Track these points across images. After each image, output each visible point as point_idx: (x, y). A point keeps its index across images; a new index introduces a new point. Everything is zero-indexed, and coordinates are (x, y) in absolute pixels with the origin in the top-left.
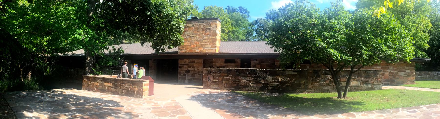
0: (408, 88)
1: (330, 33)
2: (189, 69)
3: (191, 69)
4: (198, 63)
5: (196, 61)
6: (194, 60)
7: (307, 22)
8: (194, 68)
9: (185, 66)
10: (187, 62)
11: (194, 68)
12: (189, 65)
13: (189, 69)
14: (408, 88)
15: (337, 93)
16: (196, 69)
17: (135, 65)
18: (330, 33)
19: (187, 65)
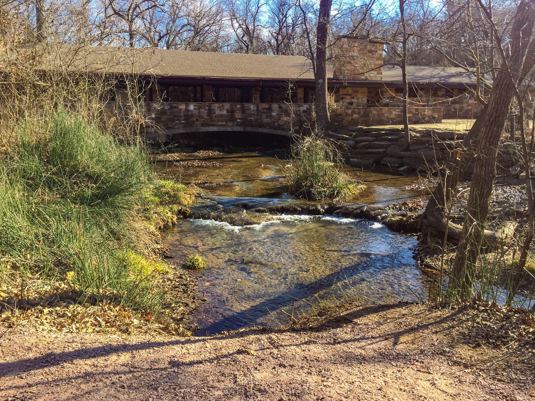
0: (230, 158)
1: (463, 43)
2: (353, 100)
3: (355, 100)
4: (362, 92)
5: (360, 90)
6: (358, 89)
7: (29, 108)
8: (358, 99)
9: (348, 97)
10: (350, 92)
11: (358, 99)
12: (353, 96)
13: (353, 100)
14: (230, 158)
15: (375, 223)
16: (360, 100)
17: (403, 126)
18: (463, 43)
19: (350, 95)
